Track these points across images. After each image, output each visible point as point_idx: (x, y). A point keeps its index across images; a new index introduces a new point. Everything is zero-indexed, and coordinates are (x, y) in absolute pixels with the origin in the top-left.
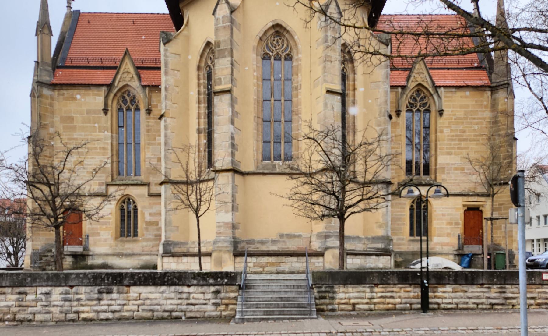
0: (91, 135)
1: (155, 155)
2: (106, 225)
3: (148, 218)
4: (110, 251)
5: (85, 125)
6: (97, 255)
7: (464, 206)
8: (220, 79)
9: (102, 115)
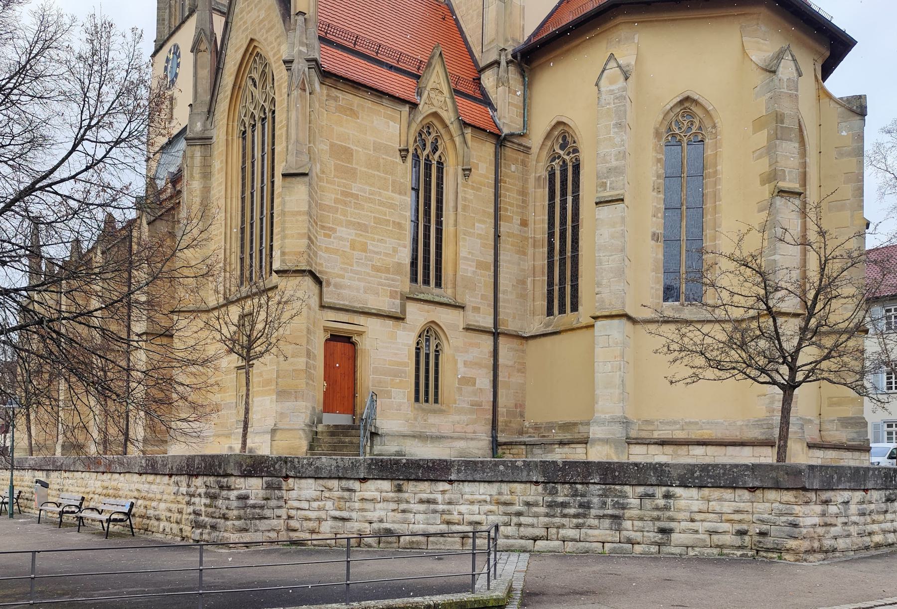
0: (380, 194)
1: (472, 254)
3: (462, 371)
4: (405, 430)
5: (370, 171)
7: (326, 329)
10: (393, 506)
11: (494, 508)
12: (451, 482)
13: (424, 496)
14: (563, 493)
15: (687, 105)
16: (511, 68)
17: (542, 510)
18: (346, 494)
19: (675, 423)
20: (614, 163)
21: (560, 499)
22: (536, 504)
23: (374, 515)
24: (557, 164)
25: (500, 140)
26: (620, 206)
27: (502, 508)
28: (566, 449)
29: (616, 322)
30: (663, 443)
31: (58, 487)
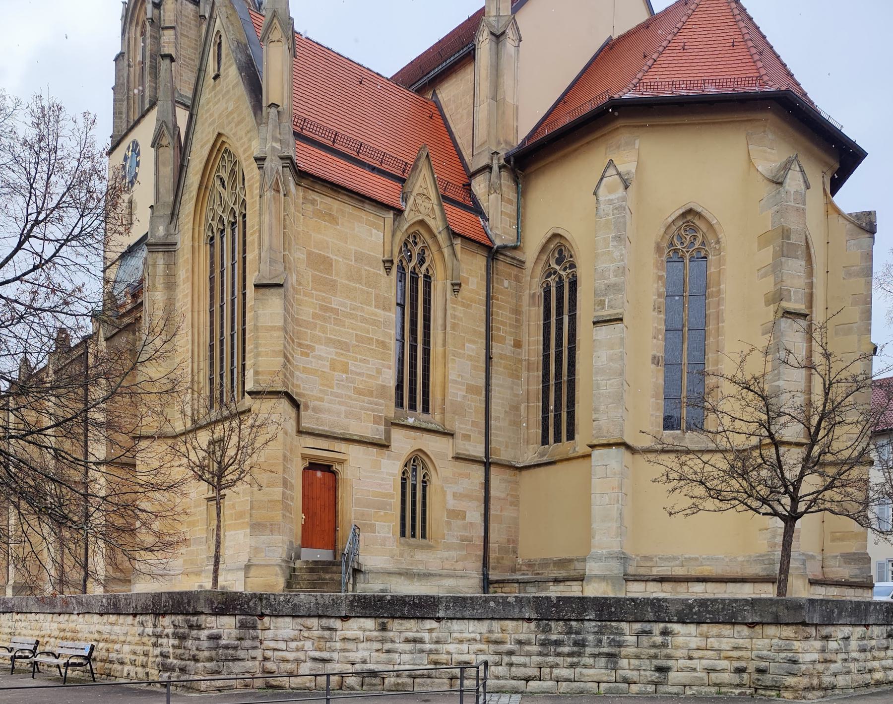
0: (362, 310)
2: (385, 509)
3: (451, 503)
4: (391, 566)
5: (351, 284)
6: (371, 572)
8: (789, 291)
9: (382, 272)
10: (378, 646)
11: (484, 647)
12: (439, 620)
13: (410, 635)
14: (557, 631)
15: (689, 218)
16: (504, 174)
17: (535, 648)
18: (327, 634)
19: (675, 558)
20: (613, 279)
21: (554, 637)
22: (528, 643)
23: (357, 656)
24: (552, 281)
25: (493, 253)
26: (619, 326)
27: (493, 647)
30: (662, 580)
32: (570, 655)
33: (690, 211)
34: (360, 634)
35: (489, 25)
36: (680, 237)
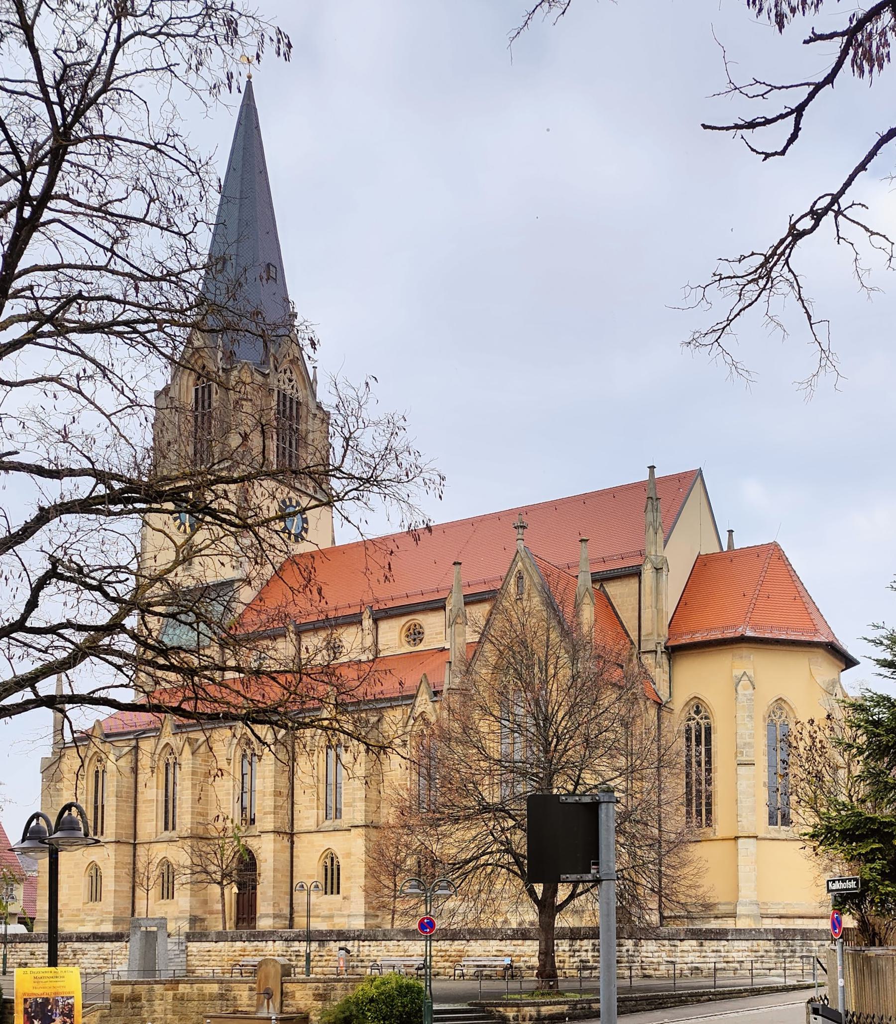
10: (698, 954)
11: (750, 954)
12: (728, 940)
13: (715, 948)
14: (783, 945)
15: (779, 702)
16: (664, 656)
17: (773, 954)
18: (673, 948)
19: (779, 904)
20: (748, 740)
21: (782, 948)
22: (770, 951)
23: (688, 960)
24: (692, 724)
26: (752, 767)
27: (754, 954)
28: (720, 921)
29: (752, 840)
30: (781, 917)
31: (299, 958)
32: (789, 957)
33: (780, 699)
34: (690, 948)
35: (651, 561)
36: (774, 712)
